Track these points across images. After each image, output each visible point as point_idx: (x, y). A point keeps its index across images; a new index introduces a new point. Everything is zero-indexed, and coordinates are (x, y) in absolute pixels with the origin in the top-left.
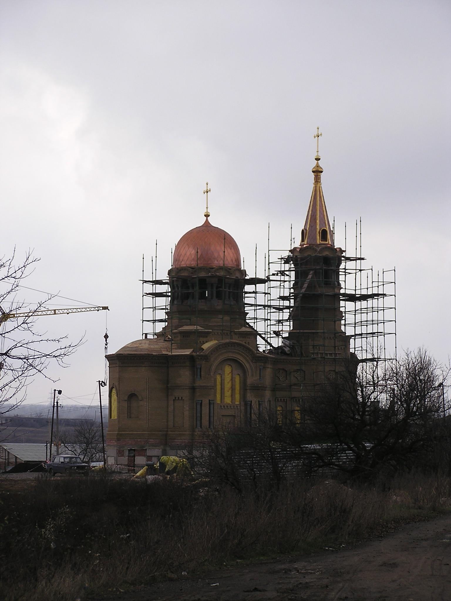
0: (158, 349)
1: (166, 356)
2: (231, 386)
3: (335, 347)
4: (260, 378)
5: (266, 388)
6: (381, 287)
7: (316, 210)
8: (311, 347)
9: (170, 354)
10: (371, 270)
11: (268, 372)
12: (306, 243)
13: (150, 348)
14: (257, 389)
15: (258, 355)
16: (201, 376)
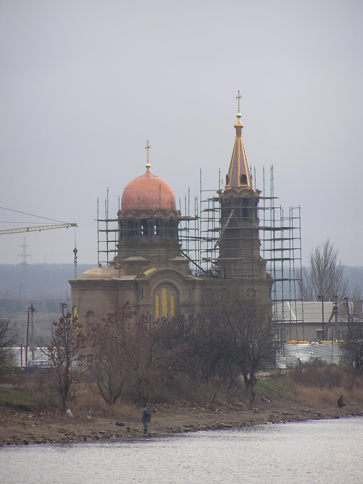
0: (110, 276)
1: (116, 282)
2: (167, 304)
3: (253, 270)
4: (190, 298)
5: (195, 304)
7: (237, 160)
8: (233, 271)
9: (119, 279)
10: (280, 208)
11: (197, 293)
12: (229, 186)
13: (103, 275)
14: (188, 305)
15: (188, 279)
16: (142, 297)
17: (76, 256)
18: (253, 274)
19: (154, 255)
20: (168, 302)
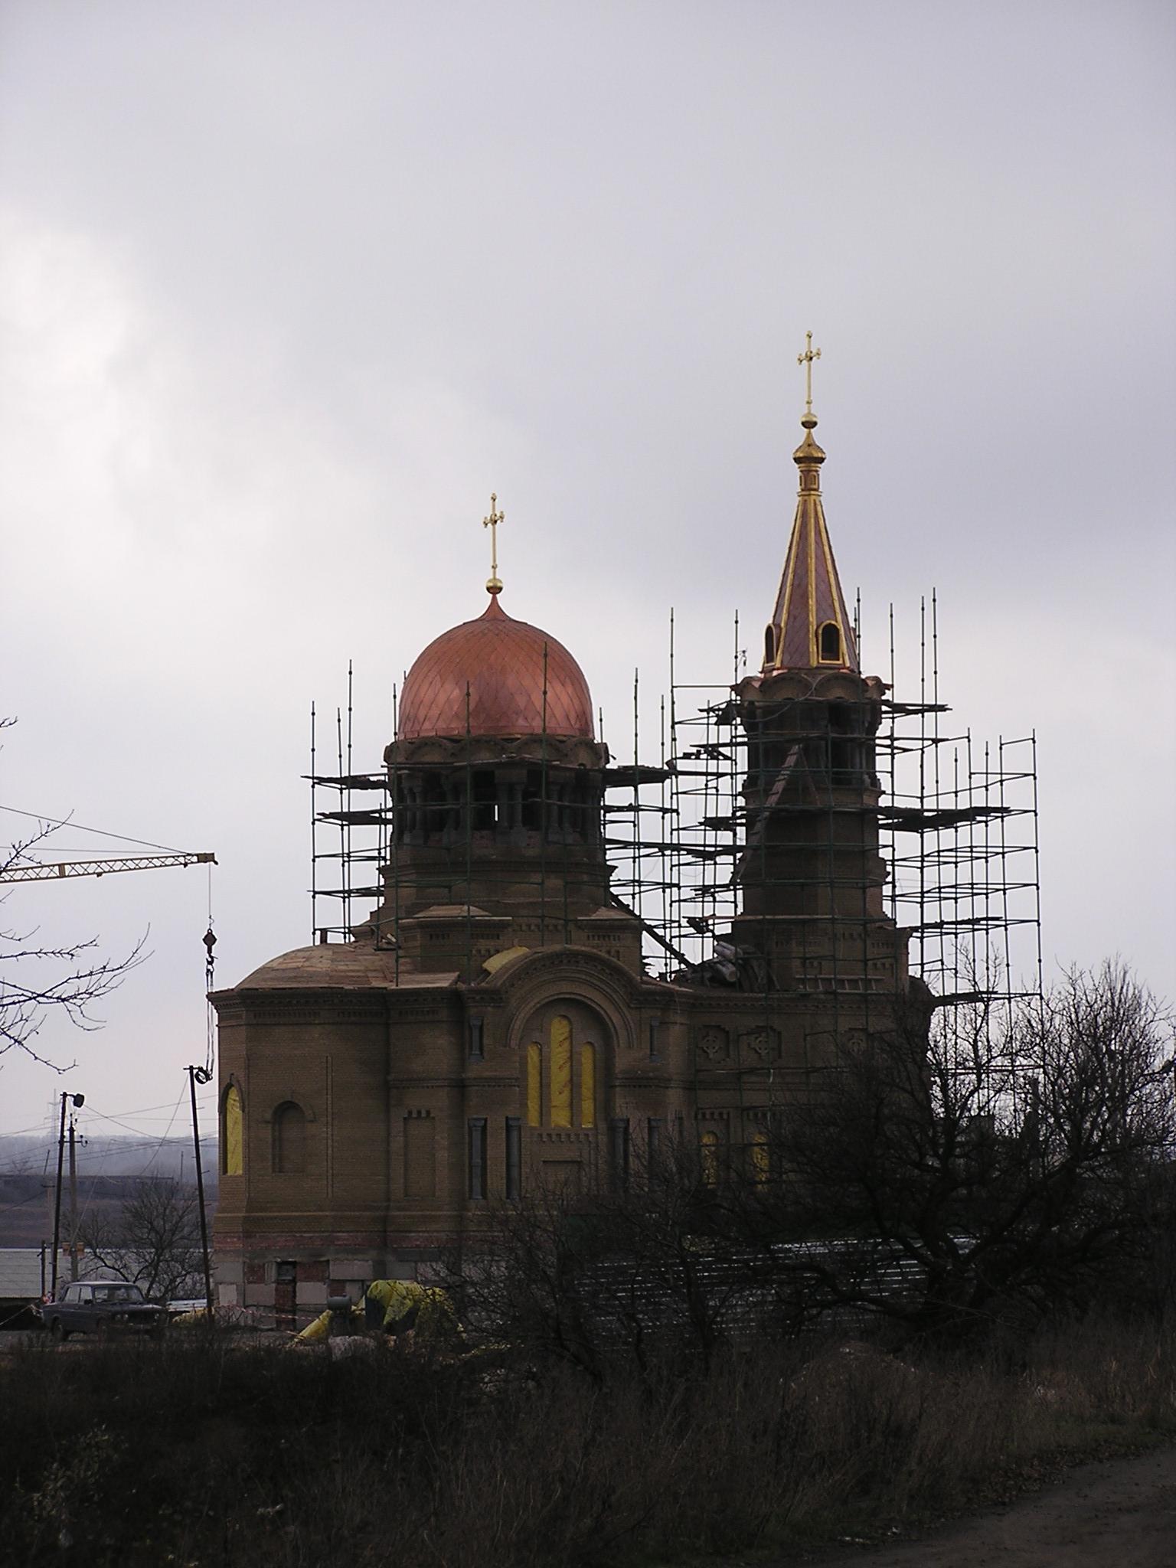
1: (382, 995)
2: (568, 1078)
3: (865, 961)
4: (651, 1055)
6: (995, 789)
7: (807, 571)
8: (798, 962)
9: (394, 987)
11: (675, 1036)
15: (644, 986)
16: (481, 1049)
17: (210, 956)
18: (866, 975)
19: (522, 900)
20: (572, 1071)
